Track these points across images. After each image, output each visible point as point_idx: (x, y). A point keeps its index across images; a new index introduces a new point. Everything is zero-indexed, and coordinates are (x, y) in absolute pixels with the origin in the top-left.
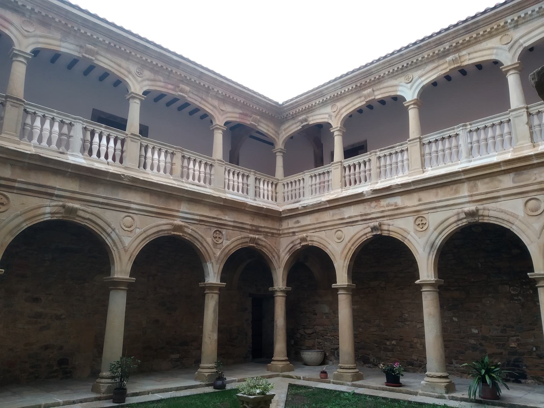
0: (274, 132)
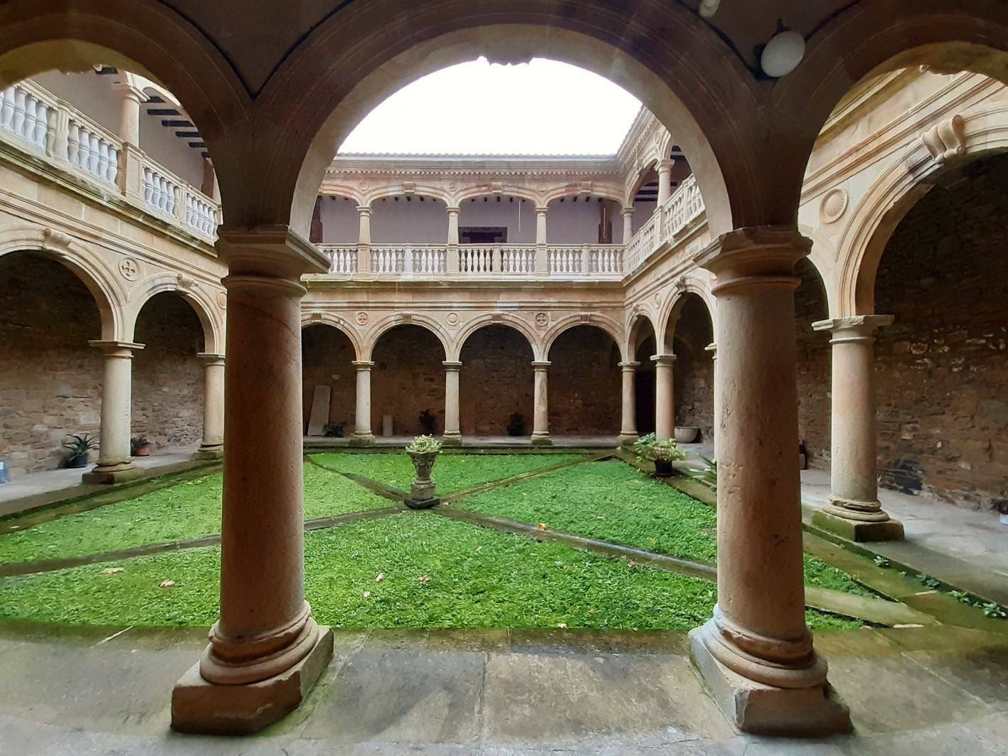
0: (616, 192)
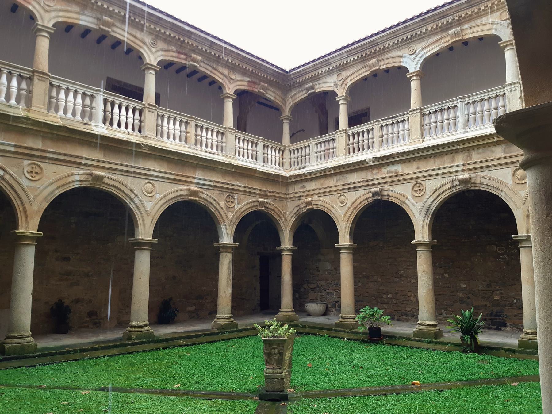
0: (281, 99)
